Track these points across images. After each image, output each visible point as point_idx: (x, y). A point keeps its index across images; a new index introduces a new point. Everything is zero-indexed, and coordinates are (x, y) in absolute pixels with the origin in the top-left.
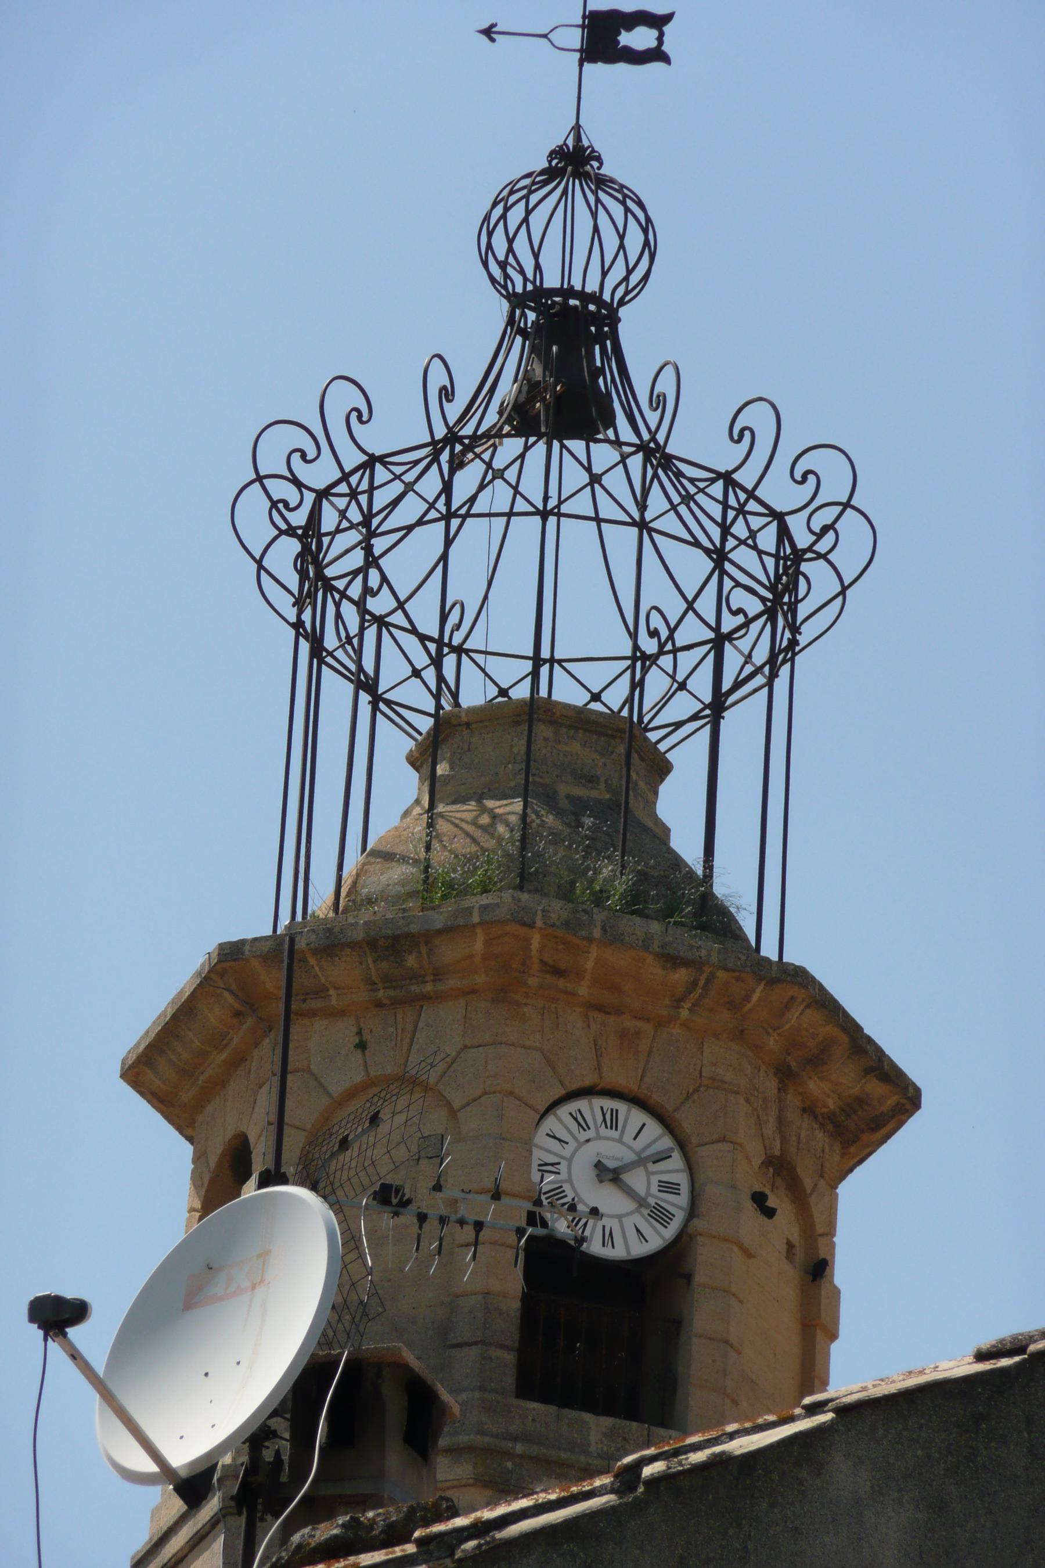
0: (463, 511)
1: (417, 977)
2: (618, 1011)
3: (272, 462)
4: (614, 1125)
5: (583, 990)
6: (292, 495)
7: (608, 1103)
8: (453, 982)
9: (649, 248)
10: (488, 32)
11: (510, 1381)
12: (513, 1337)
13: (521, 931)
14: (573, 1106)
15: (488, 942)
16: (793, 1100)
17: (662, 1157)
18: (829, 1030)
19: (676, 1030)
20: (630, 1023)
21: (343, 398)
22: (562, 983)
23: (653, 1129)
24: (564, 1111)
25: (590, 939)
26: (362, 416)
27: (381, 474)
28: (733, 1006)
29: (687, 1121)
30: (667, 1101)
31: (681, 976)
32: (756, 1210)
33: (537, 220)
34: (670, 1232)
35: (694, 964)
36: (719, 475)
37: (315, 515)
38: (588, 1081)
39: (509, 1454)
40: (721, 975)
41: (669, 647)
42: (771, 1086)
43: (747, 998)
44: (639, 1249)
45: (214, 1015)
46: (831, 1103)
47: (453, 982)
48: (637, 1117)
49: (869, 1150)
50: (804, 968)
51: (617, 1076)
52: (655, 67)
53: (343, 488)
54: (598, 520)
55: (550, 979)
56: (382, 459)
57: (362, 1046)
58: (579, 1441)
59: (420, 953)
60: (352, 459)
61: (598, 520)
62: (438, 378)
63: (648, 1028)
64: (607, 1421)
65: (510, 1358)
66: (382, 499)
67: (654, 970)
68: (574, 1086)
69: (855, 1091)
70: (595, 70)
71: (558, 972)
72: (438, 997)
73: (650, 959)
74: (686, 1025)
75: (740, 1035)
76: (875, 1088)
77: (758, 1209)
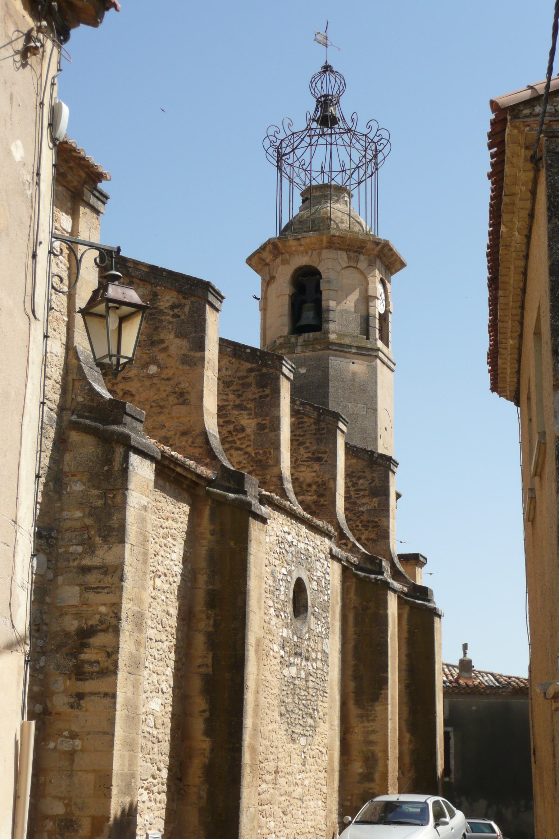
0: (316, 144)
3: (271, 133)
6: (275, 140)
9: (311, 82)
21: (287, 122)
26: (290, 125)
27: (295, 135)
32: (38, 476)
33: (337, 87)
36: (364, 135)
37: (281, 144)
41: (312, 179)
50: (488, 355)
53: (287, 139)
54: (317, 145)
56: (295, 133)
58: (60, 551)
59: (67, 233)
60: (289, 133)
61: (317, 145)
66: (295, 139)
77: (43, 479)
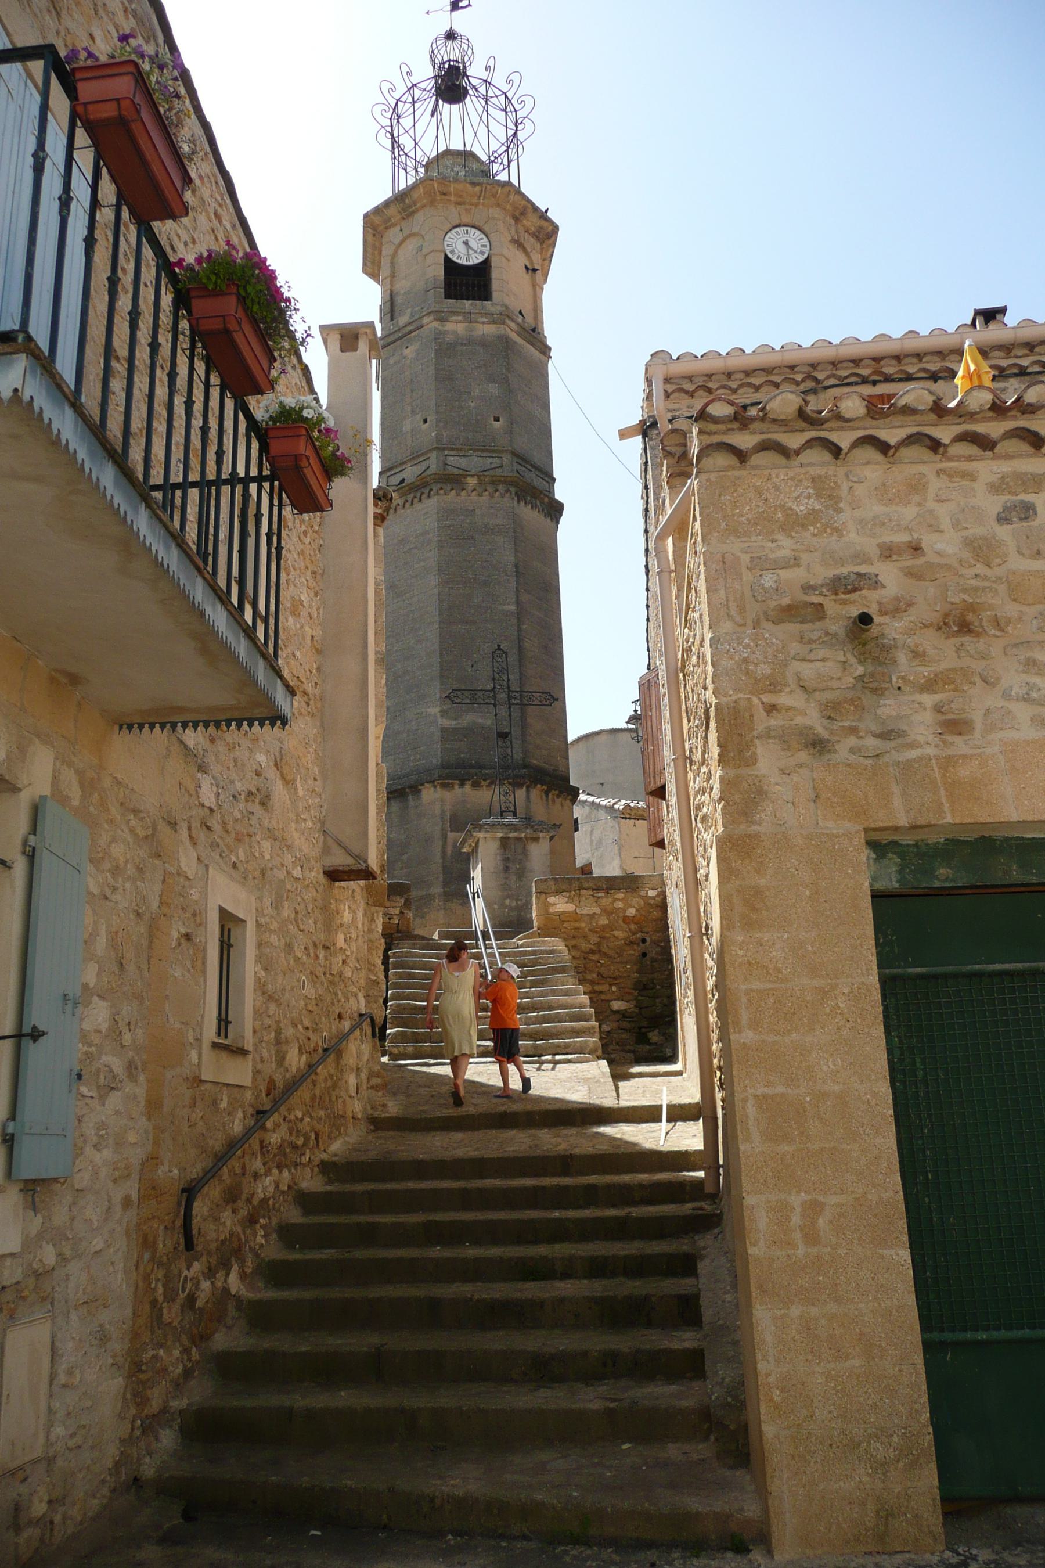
1: (410, 207)
2: (464, 203)
4: (467, 233)
5: (452, 198)
7: (465, 228)
8: (419, 205)
10: (428, 13)
11: (443, 296)
12: (443, 285)
13: (431, 182)
14: (455, 230)
15: (424, 188)
16: (521, 229)
17: (482, 239)
18: (524, 202)
19: (481, 207)
20: (467, 207)
22: (446, 197)
23: (478, 233)
24: (453, 231)
25: (450, 181)
28: (494, 196)
29: (486, 228)
30: (480, 224)
31: (478, 188)
34: (485, 256)
35: (479, 184)
38: (458, 222)
39: (443, 312)
40: (488, 187)
42: (513, 222)
43: (497, 193)
44: (477, 262)
45: (370, 238)
46: (533, 229)
47: (419, 205)
48: (473, 230)
49: (551, 250)
51: (466, 219)
52: (469, 8)
55: (443, 197)
57: (401, 230)
62: (405, 69)
63: (473, 207)
64: (470, 302)
65: (443, 290)
67: (469, 187)
68: (454, 224)
69: (538, 224)
70: (454, 13)
71: (444, 194)
72: (417, 211)
73: (468, 185)
74: (483, 204)
75: (498, 205)
76: (545, 224)
